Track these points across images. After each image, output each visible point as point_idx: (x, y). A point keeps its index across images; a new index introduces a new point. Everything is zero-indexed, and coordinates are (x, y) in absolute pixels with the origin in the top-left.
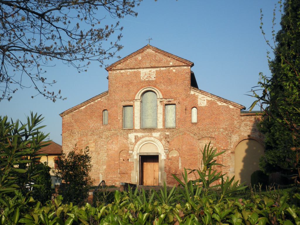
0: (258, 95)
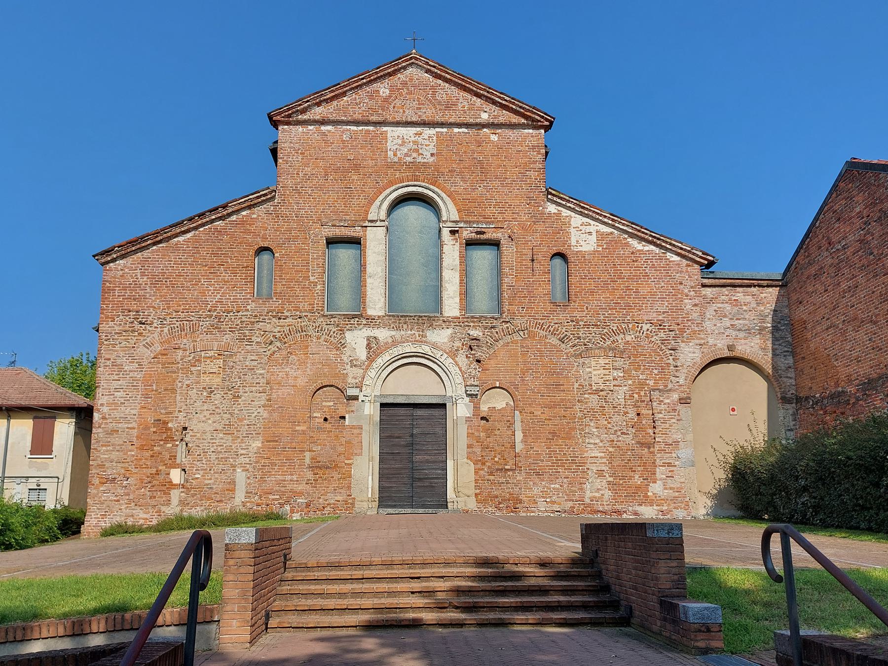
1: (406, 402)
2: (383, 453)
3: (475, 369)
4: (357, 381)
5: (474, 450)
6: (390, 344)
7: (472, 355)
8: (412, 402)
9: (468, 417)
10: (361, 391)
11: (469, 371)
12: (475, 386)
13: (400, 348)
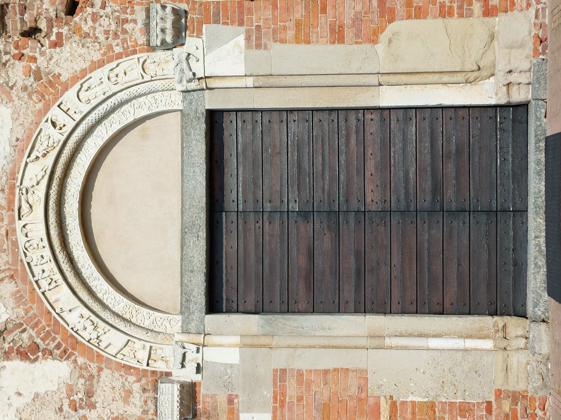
0: (11, 361)
1: (203, 234)
2: (357, 302)
3: (95, 17)
4: (136, 387)
5: (347, 21)
6: (21, 286)
7: (50, 27)
8: (203, 216)
9: (248, 39)
10: (168, 374)
11: (102, 38)
12: (148, 17)
13: (34, 256)
